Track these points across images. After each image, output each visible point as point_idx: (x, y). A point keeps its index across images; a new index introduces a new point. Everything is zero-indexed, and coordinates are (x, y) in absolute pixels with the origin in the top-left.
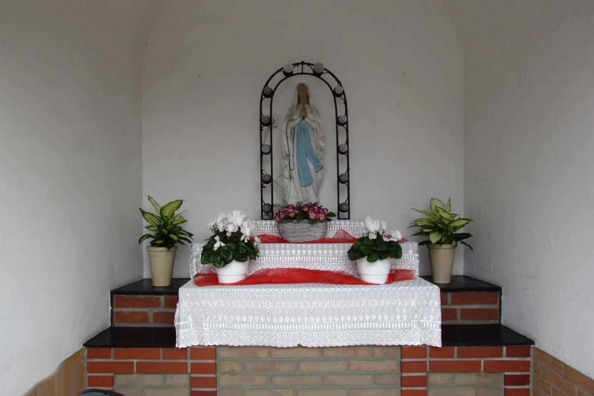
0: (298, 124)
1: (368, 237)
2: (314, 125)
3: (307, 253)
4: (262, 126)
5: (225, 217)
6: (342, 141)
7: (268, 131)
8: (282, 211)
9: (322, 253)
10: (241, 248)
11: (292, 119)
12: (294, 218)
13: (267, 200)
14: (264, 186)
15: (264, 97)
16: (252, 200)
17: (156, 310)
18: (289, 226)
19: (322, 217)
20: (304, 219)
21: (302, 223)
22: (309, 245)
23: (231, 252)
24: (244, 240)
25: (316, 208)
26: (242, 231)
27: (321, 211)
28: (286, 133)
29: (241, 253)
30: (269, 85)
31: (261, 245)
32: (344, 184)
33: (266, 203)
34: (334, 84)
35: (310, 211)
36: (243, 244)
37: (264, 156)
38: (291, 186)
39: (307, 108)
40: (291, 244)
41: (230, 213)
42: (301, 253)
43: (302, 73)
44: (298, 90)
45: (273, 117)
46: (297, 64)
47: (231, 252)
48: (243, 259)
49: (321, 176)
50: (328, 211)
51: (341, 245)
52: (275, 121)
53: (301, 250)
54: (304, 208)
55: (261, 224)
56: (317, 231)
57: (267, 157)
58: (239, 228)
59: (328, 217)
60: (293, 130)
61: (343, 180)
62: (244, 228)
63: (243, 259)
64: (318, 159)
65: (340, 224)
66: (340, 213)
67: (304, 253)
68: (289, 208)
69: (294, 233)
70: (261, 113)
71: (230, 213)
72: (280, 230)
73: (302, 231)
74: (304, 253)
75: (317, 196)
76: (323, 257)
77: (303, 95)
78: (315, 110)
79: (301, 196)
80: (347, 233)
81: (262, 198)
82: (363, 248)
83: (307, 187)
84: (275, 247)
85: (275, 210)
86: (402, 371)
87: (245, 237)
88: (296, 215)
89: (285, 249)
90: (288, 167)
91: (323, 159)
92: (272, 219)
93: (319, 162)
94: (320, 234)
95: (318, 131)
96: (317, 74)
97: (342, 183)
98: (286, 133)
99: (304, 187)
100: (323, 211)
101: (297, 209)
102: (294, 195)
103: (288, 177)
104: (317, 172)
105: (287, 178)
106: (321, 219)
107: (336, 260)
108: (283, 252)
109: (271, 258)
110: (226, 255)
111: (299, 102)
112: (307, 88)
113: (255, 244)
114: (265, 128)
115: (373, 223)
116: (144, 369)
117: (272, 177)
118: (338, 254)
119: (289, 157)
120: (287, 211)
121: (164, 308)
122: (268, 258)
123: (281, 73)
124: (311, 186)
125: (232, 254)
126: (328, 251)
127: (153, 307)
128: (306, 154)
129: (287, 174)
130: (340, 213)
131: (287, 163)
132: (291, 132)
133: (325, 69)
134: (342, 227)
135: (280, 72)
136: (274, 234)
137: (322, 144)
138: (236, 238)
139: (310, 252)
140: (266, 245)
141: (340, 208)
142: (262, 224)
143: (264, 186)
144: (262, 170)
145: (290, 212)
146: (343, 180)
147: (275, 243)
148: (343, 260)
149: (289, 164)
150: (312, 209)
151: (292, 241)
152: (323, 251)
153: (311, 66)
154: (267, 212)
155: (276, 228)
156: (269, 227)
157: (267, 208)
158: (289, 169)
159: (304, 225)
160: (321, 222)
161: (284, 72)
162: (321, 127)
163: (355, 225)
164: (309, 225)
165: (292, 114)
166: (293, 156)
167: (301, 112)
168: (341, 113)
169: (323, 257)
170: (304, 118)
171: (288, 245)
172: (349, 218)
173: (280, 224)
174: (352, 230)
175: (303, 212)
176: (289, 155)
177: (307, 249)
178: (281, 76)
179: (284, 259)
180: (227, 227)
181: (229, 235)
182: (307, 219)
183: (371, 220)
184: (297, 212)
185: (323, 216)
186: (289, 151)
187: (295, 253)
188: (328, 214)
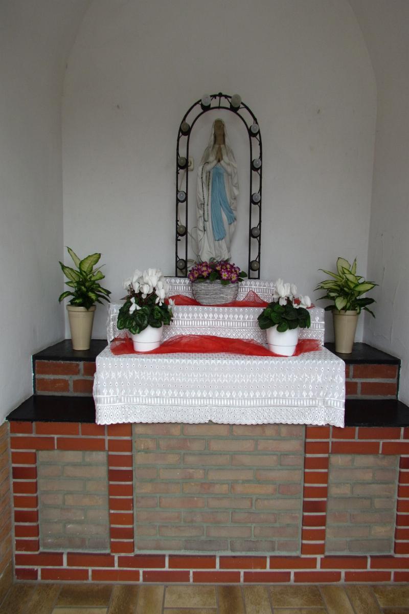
2: (229, 169)
4: (179, 169)
5: (141, 276)
6: (255, 190)
8: (196, 270)
9: (234, 318)
12: (207, 278)
13: (182, 256)
15: (181, 134)
16: (164, 251)
17: (76, 378)
18: (203, 287)
19: (234, 277)
22: (221, 309)
23: (146, 317)
24: (159, 303)
25: (228, 266)
26: (157, 292)
27: (233, 270)
28: (202, 178)
31: (175, 308)
34: (250, 121)
36: (157, 307)
37: (180, 204)
39: (223, 149)
41: (145, 271)
43: (219, 107)
45: (189, 159)
46: (214, 96)
48: (158, 325)
49: (233, 230)
51: (251, 309)
52: (191, 163)
54: (217, 266)
55: (176, 283)
56: (228, 293)
57: (182, 205)
58: (154, 289)
59: (241, 276)
60: (208, 174)
61: (254, 234)
63: (158, 325)
68: (203, 266)
71: (145, 271)
73: (215, 292)
77: (219, 134)
78: (230, 152)
80: (257, 295)
81: (176, 253)
83: (220, 241)
85: (190, 267)
86: (306, 452)
88: (209, 274)
90: (203, 218)
91: (236, 210)
92: (186, 277)
93: (232, 213)
94: (232, 297)
96: (234, 109)
98: (202, 178)
102: (207, 250)
103: (202, 229)
107: (246, 326)
109: (184, 322)
112: (223, 125)
113: (169, 307)
114: (181, 171)
115: (284, 286)
116: (65, 445)
117: (186, 228)
121: (83, 375)
122: (182, 322)
124: (223, 240)
127: (73, 374)
131: (201, 212)
132: (206, 177)
133: (242, 103)
137: (236, 192)
138: (151, 300)
140: (180, 307)
144: (177, 221)
145: (204, 271)
146: (254, 234)
147: (188, 305)
151: (203, 304)
152: (234, 315)
155: (189, 288)
156: (182, 286)
157: (181, 264)
159: (216, 286)
160: (233, 282)
166: (208, 205)
167: (217, 153)
170: (219, 161)
171: (200, 308)
172: (259, 278)
173: (194, 284)
174: (261, 292)
175: (216, 271)
176: (204, 204)
178: (198, 109)
180: (142, 288)
181: (144, 297)
183: (282, 284)
184: (210, 270)
185: (235, 276)
188: (240, 273)
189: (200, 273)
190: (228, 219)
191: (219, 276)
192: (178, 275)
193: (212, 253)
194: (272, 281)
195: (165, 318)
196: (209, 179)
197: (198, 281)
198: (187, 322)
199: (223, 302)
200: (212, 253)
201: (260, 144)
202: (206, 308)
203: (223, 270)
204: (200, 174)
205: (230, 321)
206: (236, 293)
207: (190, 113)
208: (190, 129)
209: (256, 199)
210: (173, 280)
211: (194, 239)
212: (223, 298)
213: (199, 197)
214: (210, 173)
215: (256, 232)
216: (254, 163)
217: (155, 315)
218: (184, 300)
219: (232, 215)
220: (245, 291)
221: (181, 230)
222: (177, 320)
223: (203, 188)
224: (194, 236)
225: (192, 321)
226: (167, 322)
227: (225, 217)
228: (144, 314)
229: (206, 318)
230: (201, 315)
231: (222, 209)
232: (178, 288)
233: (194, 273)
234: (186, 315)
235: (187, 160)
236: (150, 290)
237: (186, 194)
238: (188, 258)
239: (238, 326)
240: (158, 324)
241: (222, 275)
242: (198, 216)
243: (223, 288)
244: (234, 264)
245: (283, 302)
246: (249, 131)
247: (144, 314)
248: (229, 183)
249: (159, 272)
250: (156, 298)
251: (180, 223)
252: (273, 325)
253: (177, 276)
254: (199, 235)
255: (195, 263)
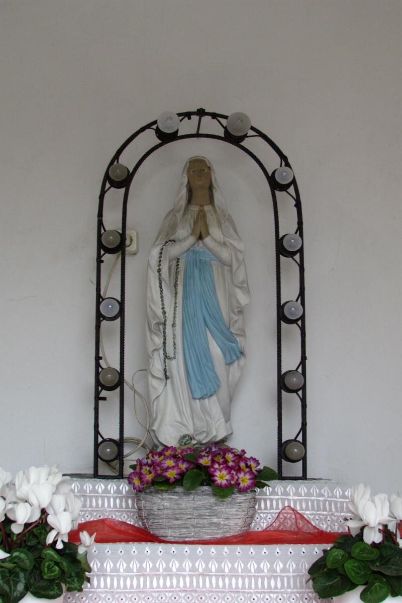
0: (188, 250)
1: (360, 536)
2: (225, 254)
3: (207, 569)
4: (102, 252)
5: (8, 480)
6: (290, 293)
7: (115, 264)
8: (147, 464)
9: (246, 570)
10: (47, 564)
11: (171, 238)
12: (179, 481)
13: (110, 431)
14: (101, 396)
15: (108, 185)
16: (71, 429)
18: (164, 503)
19: (245, 480)
20: (202, 484)
21: (196, 494)
22: (213, 549)
23: (22, 575)
24: (55, 542)
25: (230, 456)
26: (51, 520)
27: (242, 465)
28: (159, 271)
29: (45, 577)
30: (122, 160)
31: (96, 548)
32: (295, 394)
33: (105, 437)
34: (272, 162)
35: (216, 466)
36: (51, 552)
37: (104, 323)
38: (166, 396)
39: (208, 215)
40: (170, 545)
41: (21, 473)
42: (193, 569)
43: (198, 135)
44: (188, 171)
45: (127, 232)
46: (188, 115)
47: (22, 575)
48: (52, 593)
49: (237, 375)
50: (258, 464)
51: (291, 548)
52: (131, 240)
53: (193, 561)
54: (201, 457)
55: (94, 491)
56: (231, 515)
58: (44, 512)
59: (261, 478)
60: (174, 263)
61: (290, 385)
62: (55, 514)
63: (52, 593)
64: (231, 333)
65: (286, 493)
66: (284, 462)
67: (201, 570)
68: (166, 458)
69: (177, 519)
70: (100, 223)
71: (21, 473)
72: (140, 509)
73: (196, 513)
74: (201, 570)
75: (228, 419)
76: (247, 580)
77: (200, 185)
78: (226, 220)
79: (190, 421)
80: (302, 516)
81: (96, 426)
82: (350, 567)
83: (206, 400)
84: (128, 552)
85: (132, 456)
87: (58, 533)
88: (182, 475)
89: (154, 559)
90: (162, 352)
91: (243, 333)
92: (120, 476)
93: (235, 341)
94: (240, 522)
95: (235, 268)
96: (233, 138)
97: (289, 391)
98: (159, 271)
99: (198, 401)
100: (247, 466)
101: (184, 461)
102: (175, 420)
103: (161, 375)
104: (229, 364)
105: (158, 378)
106: (242, 485)
107: (279, 586)
108: (148, 565)
109: (119, 581)
110: (8, 582)
111: (189, 201)
112: (209, 168)
113: (81, 550)
114: (107, 257)
115: (373, 501)
117: (121, 374)
118: (282, 571)
119: (165, 329)
120: (159, 464)
122: (112, 581)
123: (150, 134)
124: (214, 398)
125: (23, 580)
126: (258, 564)
128: (205, 321)
129: (157, 366)
130: (284, 462)
131: (159, 341)
132: (170, 268)
133: (253, 128)
134: (289, 500)
135: (148, 131)
136: (131, 522)
137: (242, 298)
138: (35, 536)
139: (213, 566)
140: (108, 547)
141: (284, 451)
142: (97, 492)
143: (101, 396)
144: (98, 358)
145: (168, 468)
146: (290, 385)
147: (127, 541)
148: (295, 587)
149: (164, 343)
150: (221, 461)
151: (167, 539)
152: (246, 563)
153: (219, 119)
154: (108, 459)
155: (130, 502)
156: (112, 499)
157: (108, 451)
158: (162, 356)
159: (202, 499)
160: (243, 491)
161: (158, 132)
162: (240, 257)
163: (321, 495)
164: (212, 500)
165: (173, 228)
166: (174, 325)
167: (195, 223)
168: (288, 226)
169: (247, 580)
170: (200, 238)
171: (160, 547)
172: (304, 477)
173: (142, 495)
174: (313, 509)
175: (199, 467)
176: (164, 324)
177: (207, 559)
178: (149, 139)
179: (151, 582)
180: (12, 510)
181: (16, 529)
182: (208, 485)
183: (368, 496)
184: (183, 466)
185: (248, 476)
186: (164, 313)
187: (178, 570)
188: (259, 471)
189: (159, 472)
190: (225, 356)
191: (209, 480)
192: (100, 473)
193: (185, 426)
194: (338, 484)
195: (71, 576)
196: (177, 273)
197: (152, 489)
198: (125, 581)
199: (217, 534)
200: (185, 426)
201: (298, 205)
202: (173, 548)
203: (216, 466)
204: (154, 262)
205: (237, 577)
206: (251, 512)
207: (143, 163)
208: (130, 176)
209: (293, 311)
210: (88, 485)
211: (140, 395)
212: (217, 525)
213: (152, 309)
214: (178, 262)
215: (294, 381)
216: (285, 244)
217: (46, 570)
218: (120, 531)
219: (233, 345)
220: (272, 507)
221: (108, 379)
222: (98, 576)
223: (161, 291)
224: (138, 388)
225: (138, 577)
226: (76, 585)
227: (216, 350)
228: (18, 570)
229: (174, 570)
230: (161, 566)
231: (208, 333)
232: (100, 502)
233: (143, 471)
234: (122, 566)
235: (123, 236)
236: (32, 512)
237: (122, 304)
238: (126, 435)
239: (257, 587)
240: (53, 590)
241: (214, 476)
242: (151, 348)
243: (216, 505)
244: (244, 452)
245: (373, 537)
246: (272, 180)
247: (18, 570)
248: (224, 280)
249: (55, 474)
250: (47, 533)
251: (106, 361)
252: (352, 586)
253: (96, 475)
254: (154, 388)
255: (143, 446)
